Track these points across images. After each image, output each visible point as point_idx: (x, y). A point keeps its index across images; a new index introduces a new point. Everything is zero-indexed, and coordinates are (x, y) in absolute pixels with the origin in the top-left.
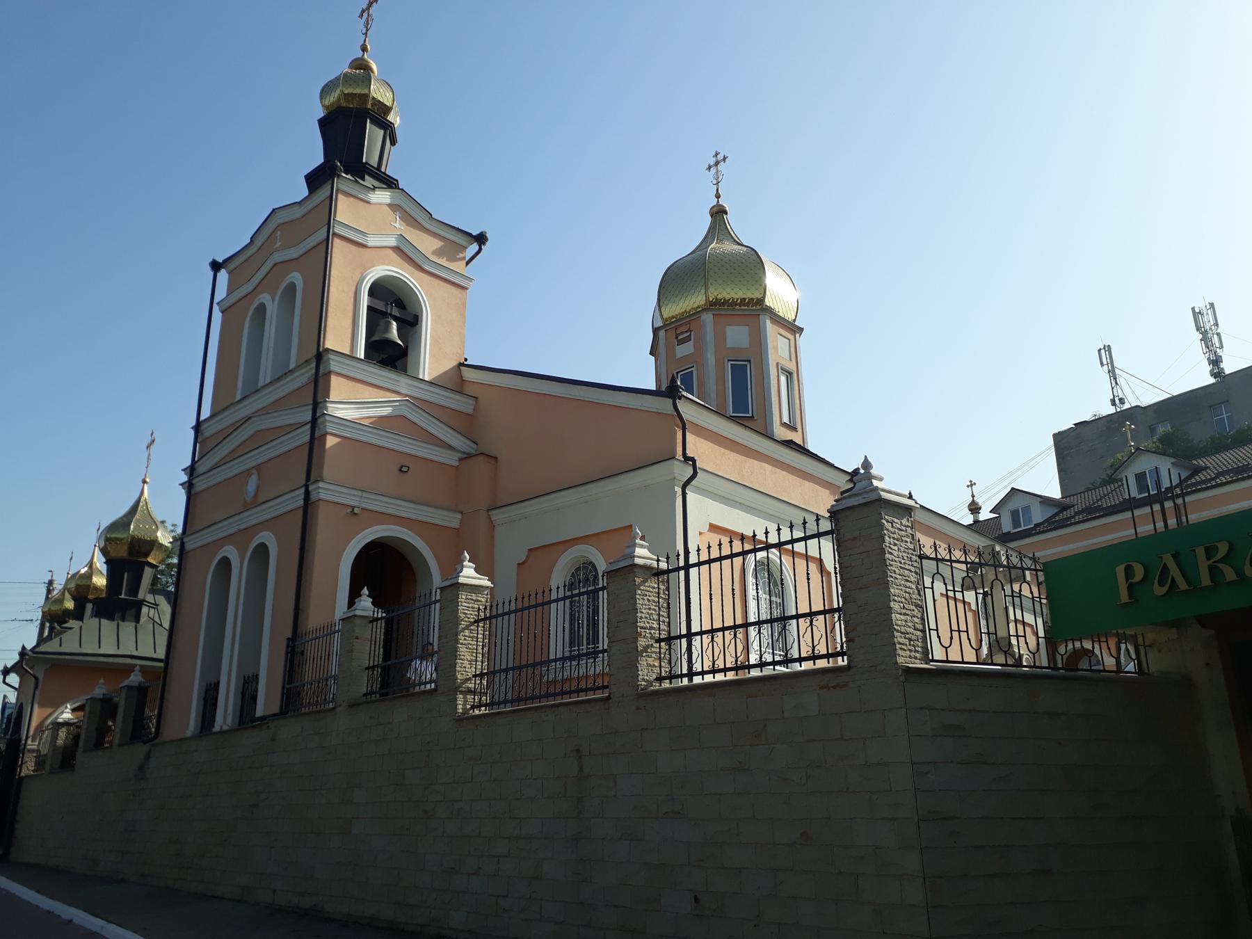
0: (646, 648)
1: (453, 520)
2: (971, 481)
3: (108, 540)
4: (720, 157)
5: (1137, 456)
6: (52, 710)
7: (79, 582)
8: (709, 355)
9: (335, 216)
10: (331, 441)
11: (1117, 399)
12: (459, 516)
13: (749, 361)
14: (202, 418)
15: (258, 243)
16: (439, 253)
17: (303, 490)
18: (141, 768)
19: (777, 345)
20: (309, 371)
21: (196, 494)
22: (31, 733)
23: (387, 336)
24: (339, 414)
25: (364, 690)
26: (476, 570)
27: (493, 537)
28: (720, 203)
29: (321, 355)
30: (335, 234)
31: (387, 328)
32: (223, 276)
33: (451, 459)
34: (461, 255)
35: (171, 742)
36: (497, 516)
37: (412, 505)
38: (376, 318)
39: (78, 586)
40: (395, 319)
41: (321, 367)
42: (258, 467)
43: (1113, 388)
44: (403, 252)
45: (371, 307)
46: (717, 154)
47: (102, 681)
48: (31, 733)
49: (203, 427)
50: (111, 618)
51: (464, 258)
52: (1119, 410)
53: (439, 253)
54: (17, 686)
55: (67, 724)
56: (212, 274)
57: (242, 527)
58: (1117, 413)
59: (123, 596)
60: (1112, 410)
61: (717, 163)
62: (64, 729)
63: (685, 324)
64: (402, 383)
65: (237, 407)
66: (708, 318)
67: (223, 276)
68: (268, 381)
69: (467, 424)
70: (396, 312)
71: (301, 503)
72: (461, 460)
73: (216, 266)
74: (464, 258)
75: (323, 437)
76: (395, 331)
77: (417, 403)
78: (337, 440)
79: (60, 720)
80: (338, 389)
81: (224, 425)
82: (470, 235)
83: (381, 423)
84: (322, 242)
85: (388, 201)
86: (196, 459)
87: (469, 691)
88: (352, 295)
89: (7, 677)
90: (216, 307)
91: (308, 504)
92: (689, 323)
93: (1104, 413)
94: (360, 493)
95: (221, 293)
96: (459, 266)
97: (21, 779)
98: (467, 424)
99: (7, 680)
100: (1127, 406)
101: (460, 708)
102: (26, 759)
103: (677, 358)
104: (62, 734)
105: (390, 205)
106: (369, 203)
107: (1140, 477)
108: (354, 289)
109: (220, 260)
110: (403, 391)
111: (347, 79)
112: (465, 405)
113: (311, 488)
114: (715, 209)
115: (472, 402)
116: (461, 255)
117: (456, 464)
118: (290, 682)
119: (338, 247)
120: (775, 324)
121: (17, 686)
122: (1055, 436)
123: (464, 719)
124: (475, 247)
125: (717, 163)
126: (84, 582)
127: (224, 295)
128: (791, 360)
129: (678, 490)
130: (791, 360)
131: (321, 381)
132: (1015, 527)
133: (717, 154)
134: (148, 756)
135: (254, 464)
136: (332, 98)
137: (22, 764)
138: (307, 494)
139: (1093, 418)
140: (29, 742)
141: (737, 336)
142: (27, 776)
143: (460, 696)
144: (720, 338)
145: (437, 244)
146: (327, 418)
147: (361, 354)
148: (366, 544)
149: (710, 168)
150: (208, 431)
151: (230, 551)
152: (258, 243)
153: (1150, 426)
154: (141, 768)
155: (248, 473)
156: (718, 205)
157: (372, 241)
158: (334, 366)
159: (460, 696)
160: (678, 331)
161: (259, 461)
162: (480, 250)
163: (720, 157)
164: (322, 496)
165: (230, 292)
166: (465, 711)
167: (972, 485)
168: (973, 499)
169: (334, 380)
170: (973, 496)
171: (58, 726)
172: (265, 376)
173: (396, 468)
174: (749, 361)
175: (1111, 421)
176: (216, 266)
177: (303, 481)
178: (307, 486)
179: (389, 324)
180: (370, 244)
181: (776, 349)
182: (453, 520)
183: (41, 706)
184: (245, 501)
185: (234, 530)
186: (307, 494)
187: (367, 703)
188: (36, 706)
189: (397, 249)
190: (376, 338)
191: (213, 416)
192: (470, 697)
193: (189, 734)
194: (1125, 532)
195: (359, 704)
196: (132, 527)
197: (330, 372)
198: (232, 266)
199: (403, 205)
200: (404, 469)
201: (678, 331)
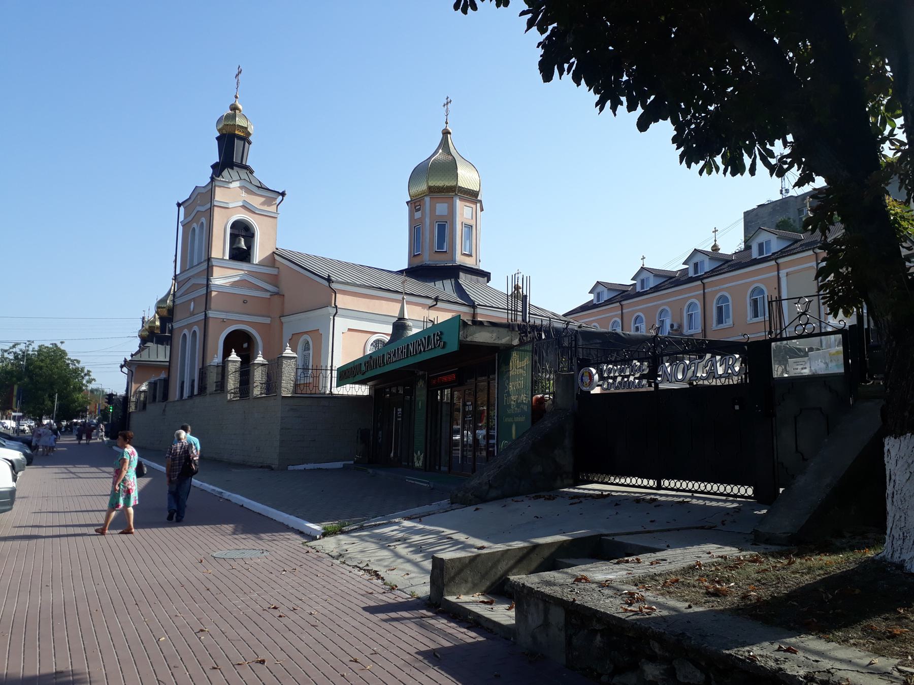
0: (257, 386)
1: (267, 321)
2: (643, 256)
3: (158, 308)
4: (449, 100)
5: (759, 234)
6: (139, 385)
7: (150, 325)
8: (427, 220)
9: (214, 198)
10: (214, 294)
11: (783, 190)
12: (270, 319)
13: (447, 222)
14: (177, 273)
15: (193, 199)
16: (263, 204)
17: (204, 313)
18: (164, 410)
19: (463, 211)
20: (205, 266)
21: (177, 305)
22: (132, 394)
23: (240, 246)
24: (216, 283)
25: (214, 389)
26: (237, 355)
27: (282, 328)
28: (448, 128)
29: (209, 259)
30: (214, 206)
31: (239, 242)
32: (182, 208)
33: (267, 295)
34: (274, 202)
35: (171, 402)
36: (283, 319)
37: (248, 316)
38: (234, 238)
39: (150, 327)
40: (243, 237)
41: (210, 263)
42: (194, 299)
43: (782, 182)
44: (246, 207)
45: (234, 234)
46: (447, 98)
47: (163, 372)
48: (132, 394)
49: (177, 277)
50: (162, 344)
51: (276, 203)
52: (784, 197)
53: (263, 204)
54: (127, 373)
55: (144, 391)
56: (177, 208)
57: (189, 323)
58: (783, 199)
59: (167, 334)
60: (780, 197)
61: (447, 103)
62: (143, 394)
63: (418, 201)
64: (245, 266)
65: (188, 272)
66: (427, 199)
67: (182, 208)
68: (196, 264)
69: (274, 280)
70: (243, 234)
71: (204, 318)
72: (271, 295)
73: (179, 205)
74: (276, 203)
75: (211, 291)
76: (243, 243)
77: (251, 273)
78: (216, 293)
79: (141, 390)
80: (217, 272)
81: (185, 278)
82: (278, 192)
83: (234, 284)
84: (207, 210)
85: (239, 185)
86: (176, 290)
87: (232, 393)
88: (223, 230)
89: (123, 369)
90: (180, 223)
91: (206, 318)
92: (420, 201)
93: (774, 200)
94: (225, 314)
95: (182, 218)
96: (273, 209)
97: (130, 413)
98: (274, 280)
99: (123, 371)
100: (789, 195)
101: (229, 398)
102: (131, 405)
103: (415, 218)
104: (142, 395)
105: (239, 187)
106: (229, 188)
107: (761, 246)
108: (224, 227)
109: (180, 202)
110: (245, 269)
111: (228, 117)
112: (273, 271)
113: (207, 312)
114: (444, 131)
115: (277, 270)
116: (274, 202)
117: (269, 297)
118: (202, 384)
119: (217, 211)
120: (463, 201)
121: (127, 373)
122: (745, 213)
123: (230, 401)
124: (281, 197)
125: (447, 103)
126: (152, 325)
127: (183, 219)
128: (472, 219)
129: (332, 317)
130: (472, 219)
131: (210, 270)
132: (695, 274)
133: (447, 98)
134: (166, 405)
135: (193, 297)
136: (221, 126)
137: (130, 407)
138: (206, 315)
139: (767, 203)
140: (132, 398)
141: (441, 208)
142: (132, 412)
143: (229, 395)
144: (433, 210)
145: (262, 199)
146: (211, 285)
147: (227, 257)
148: (228, 335)
149: (444, 105)
150: (180, 279)
151: (186, 331)
152: (193, 199)
153: (798, 209)
154: (164, 410)
155: (190, 301)
156: (446, 129)
157: (231, 206)
158: (214, 263)
159: (229, 395)
160: (416, 204)
161: (195, 296)
162: (283, 199)
163: (449, 100)
164: (210, 316)
165: (185, 218)
166: (231, 399)
167: (643, 258)
168: (715, 243)
169: (215, 268)
170: (715, 241)
171: (141, 392)
172: (195, 263)
173: (242, 302)
174: (447, 222)
175: (776, 204)
176: (179, 205)
177: (204, 310)
178: (205, 312)
179: (240, 240)
180: (230, 207)
181: (462, 214)
182: (267, 321)
183: (135, 383)
184: (190, 312)
185: (186, 324)
186: (206, 315)
187: (214, 394)
188: (133, 383)
189: (244, 207)
190: (234, 247)
191: (180, 273)
192: (232, 395)
193: (176, 399)
194: (793, 268)
195: (212, 394)
196: (168, 301)
197: (213, 266)
198: (187, 204)
199: (245, 186)
200: (245, 302)
201: (416, 204)
